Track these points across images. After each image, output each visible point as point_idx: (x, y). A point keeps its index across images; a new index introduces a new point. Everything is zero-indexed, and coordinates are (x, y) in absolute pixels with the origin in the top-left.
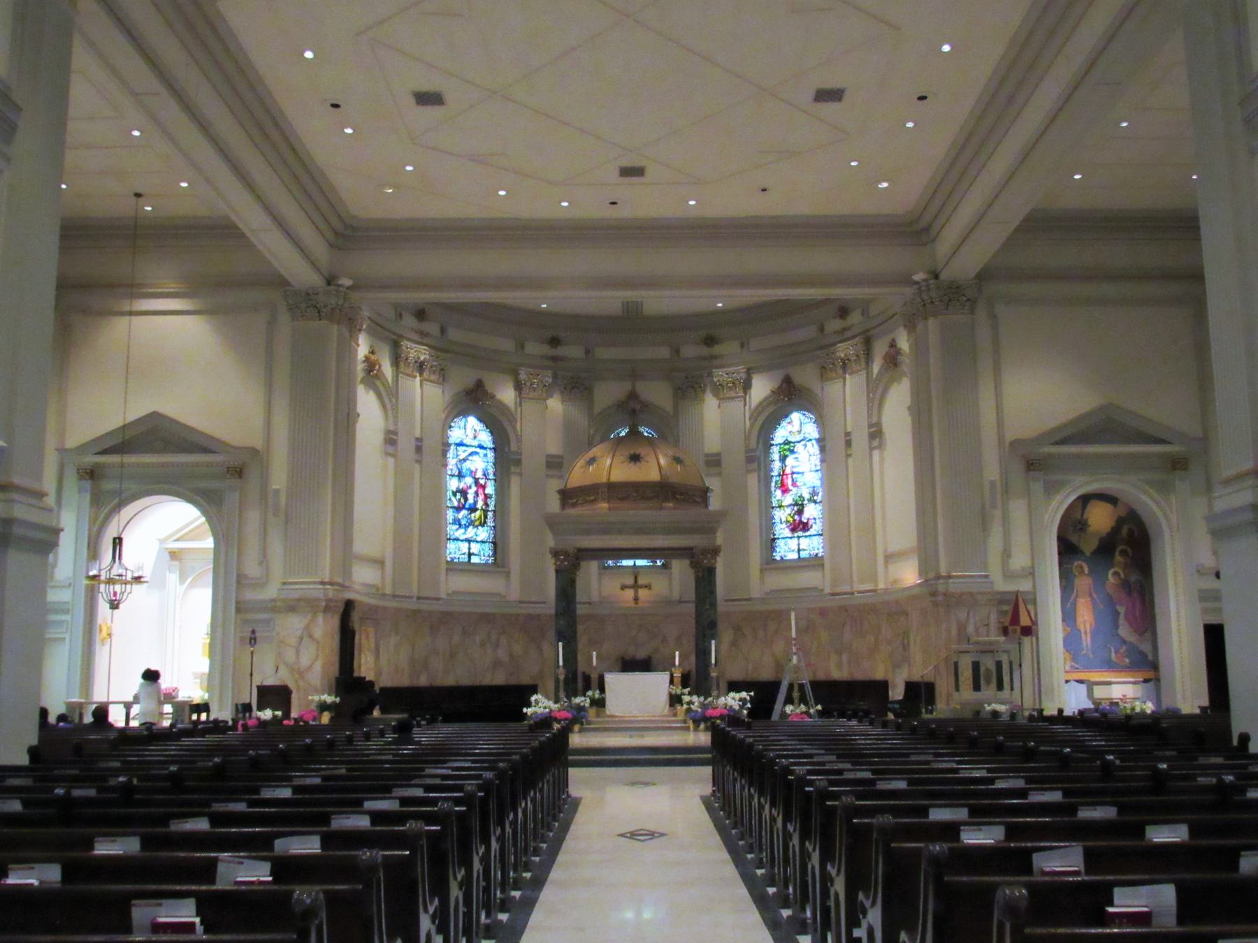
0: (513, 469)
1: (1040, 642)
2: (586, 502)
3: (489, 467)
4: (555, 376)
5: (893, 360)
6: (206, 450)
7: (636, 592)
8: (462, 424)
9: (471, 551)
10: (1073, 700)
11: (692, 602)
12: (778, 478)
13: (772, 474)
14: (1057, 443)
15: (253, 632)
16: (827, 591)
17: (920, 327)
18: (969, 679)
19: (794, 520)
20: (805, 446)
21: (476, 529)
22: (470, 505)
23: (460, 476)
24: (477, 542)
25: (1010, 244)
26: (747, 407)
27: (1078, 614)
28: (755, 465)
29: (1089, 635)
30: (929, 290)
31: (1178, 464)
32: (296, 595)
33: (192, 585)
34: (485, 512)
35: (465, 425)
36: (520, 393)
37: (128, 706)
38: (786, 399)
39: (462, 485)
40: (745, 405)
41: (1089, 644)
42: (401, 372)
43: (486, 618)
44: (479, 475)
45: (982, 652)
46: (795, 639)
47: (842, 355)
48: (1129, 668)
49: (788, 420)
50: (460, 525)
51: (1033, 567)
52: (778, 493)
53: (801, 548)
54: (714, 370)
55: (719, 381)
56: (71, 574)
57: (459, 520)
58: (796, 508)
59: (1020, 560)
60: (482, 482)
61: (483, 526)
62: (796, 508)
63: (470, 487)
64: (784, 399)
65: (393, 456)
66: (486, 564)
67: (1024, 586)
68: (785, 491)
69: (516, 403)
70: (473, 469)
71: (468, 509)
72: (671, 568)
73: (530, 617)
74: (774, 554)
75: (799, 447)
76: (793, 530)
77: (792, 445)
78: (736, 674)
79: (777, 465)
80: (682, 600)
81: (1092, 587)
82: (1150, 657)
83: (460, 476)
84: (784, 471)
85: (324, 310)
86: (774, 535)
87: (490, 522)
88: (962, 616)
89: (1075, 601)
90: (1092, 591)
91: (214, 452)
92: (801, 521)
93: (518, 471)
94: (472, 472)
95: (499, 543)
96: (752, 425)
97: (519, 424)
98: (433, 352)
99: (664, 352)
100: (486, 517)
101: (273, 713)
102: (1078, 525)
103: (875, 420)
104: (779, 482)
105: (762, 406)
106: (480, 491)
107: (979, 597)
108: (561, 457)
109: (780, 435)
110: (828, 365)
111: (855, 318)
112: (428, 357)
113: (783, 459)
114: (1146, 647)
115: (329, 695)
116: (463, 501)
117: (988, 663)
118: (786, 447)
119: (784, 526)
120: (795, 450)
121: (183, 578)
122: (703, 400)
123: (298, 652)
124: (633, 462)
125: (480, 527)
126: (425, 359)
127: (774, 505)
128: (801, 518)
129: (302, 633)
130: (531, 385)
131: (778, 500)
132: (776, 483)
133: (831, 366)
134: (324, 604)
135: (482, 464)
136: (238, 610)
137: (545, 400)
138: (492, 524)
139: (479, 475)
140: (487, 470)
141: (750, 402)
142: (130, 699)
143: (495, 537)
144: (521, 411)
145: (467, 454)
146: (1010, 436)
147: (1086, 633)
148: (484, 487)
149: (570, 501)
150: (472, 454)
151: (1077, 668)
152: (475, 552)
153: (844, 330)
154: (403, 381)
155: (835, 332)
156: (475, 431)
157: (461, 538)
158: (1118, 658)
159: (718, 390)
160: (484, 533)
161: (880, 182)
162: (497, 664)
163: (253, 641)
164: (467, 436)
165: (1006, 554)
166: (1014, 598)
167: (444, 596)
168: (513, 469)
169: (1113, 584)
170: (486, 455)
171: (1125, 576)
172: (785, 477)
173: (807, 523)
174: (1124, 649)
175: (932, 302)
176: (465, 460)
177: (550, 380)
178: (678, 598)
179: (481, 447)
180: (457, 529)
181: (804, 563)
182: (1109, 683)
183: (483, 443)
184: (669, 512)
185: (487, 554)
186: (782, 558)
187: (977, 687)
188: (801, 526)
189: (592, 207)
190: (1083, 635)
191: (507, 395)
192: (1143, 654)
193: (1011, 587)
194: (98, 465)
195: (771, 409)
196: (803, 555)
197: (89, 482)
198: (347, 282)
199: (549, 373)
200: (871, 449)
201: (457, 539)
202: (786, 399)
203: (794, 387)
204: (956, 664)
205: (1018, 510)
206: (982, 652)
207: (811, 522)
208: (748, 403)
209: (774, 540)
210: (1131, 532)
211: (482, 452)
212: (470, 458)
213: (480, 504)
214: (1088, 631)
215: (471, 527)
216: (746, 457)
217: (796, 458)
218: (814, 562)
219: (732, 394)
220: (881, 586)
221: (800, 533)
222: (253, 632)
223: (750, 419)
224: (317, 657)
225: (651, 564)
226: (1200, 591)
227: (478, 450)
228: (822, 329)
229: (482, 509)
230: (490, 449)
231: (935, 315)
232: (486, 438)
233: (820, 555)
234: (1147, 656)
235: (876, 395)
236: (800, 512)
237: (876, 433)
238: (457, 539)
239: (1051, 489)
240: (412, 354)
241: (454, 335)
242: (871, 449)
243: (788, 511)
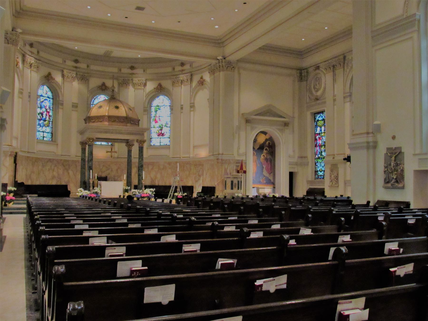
0: (60, 107)
1: (247, 176)
2: (99, 121)
3: (51, 105)
4: (77, 74)
5: (202, 82)
6: (281, 117)
7: (112, 154)
8: (42, 88)
9: (44, 136)
10: (252, 193)
11: (126, 158)
12: (154, 118)
13: (152, 116)
14: (255, 115)
16: (171, 156)
17: (216, 74)
18: (230, 186)
19: (159, 132)
20: (164, 107)
21: (46, 128)
22: (44, 119)
23: (41, 108)
24: (46, 132)
25: (256, 52)
26: (145, 93)
28: (146, 113)
29: (255, 174)
30: (222, 62)
31: (286, 124)
34: (49, 121)
35: (43, 89)
36: (64, 79)
38: (159, 91)
39: (41, 111)
40: (144, 91)
41: (255, 176)
42: (25, 67)
43: (50, 160)
44: (47, 108)
45: (234, 178)
46: (178, 172)
47: (182, 79)
48: (265, 184)
49: (158, 98)
50: (40, 126)
51: (246, 153)
52: (154, 122)
53: (161, 142)
54: (134, 78)
55: (135, 82)
57: (40, 124)
58: (160, 128)
59: (242, 150)
60: (48, 110)
61: (48, 127)
62: (160, 128)
63: (44, 112)
64: (158, 91)
65: (21, 98)
66: (49, 141)
67: (243, 158)
68: (156, 122)
69: (62, 83)
70: (46, 106)
71: (43, 120)
72: (115, 146)
73: (65, 161)
74: (151, 143)
75: (162, 108)
76: (159, 135)
77: (159, 107)
78: (148, 183)
79: (153, 114)
80: (119, 157)
82: (272, 181)
83: (41, 108)
84: (156, 115)
85: (10, 40)
86: (151, 137)
87: (50, 125)
88: (226, 167)
91: (284, 118)
92: (161, 133)
93: (62, 107)
94: (45, 106)
95: (53, 133)
96: (146, 99)
97: (63, 90)
98: (36, 60)
99: (115, 70)
100: (49, 124)
103: (192, 102)
104: (154, 119)
105: (150, 93)
106: (48, 114)
107: (231, 161)
108: (77, 104)
109: (156, 102)
110: (176, 82)
111: (187, 67)
112: (34, 62)
113: (156, 111)
114: (271, 178)
115: (12, 187)
116: (42, 117)
117: (235, 181)
118: (158, 107)
119: (155, 134)
120: (161, 109)
122: (129, 88)
124: (116, 109)
125: (47, 127)
126: (33, 62)
127: (152, 127)
128: (161, 132)
130: (68, 76)
131: (154, 125)
132: (153, 119)
133: (177, 82)
134: (10, 153)
135: (48, 104)
137: (72, 82)
138: (51, 126)
139: (47, 108)
140: (50, 106)
141: (146, 91)
143: (52, 131)
144: (64, 86)
145: (43, 99)
146: (242, 111)
148: (49, 112)
149: (92, 121)
150: (45, 100)
152: (46, 136)
153: (183, 70)
154: (26, 69)
155: (179, 71)
156: (46, 91)
157: (41, 131)
159: (134, 85)
160: (48, 129)
161: (216, 25)
162: (53, 177)
164: (44, 93)
165: (239, 148)
166: (241, 162)
167: (36, 152)
168: (60, 107)
170: (50, 101)
171: (266, 156)
172: (156, 117)
173: (164, 134)
174: (264, 178)
175: (223, 67)
176: (42, 102)
177: (75, 75)
178: (117, 157)
179: (48, 97)
180: (39, 127)
181: (161, 147)
182: (264, 188)
183: (49, 96)
184: (130, 128)
185: (49, 137)
186: (154, 145)
187: (232, 188)
188: (161, 134)
189: (119, 18)
191: (58, 78)
192: (270, 180)
193: (240, 158)
195: (154, 94)
196: (162, 144)
198: (19, 31)
199: (75, 73)
200: (190, 111)
201: (39, 131)
202: (159, 91)
203: (162, 87)
204: (226, 181)
205: (243, 134)
206: (234, 178)
207: (165, 134)
208: (145, 91)
209: (151, 138)
210: (269, 143)
211: (49, 99)
212: (44, 101)
213: (47, 119)
214: (255, 172)
215: (44, 127)
216: (144, 110)
217: (161, 111)
218: (167, 147)
219: (140, 87)
220: (191, 156)
221: (161, 137)
223: (145, 97)
225: (107, 144)
226: (289, 162)
227: (47, 98)
228: (174, 69)
229: (48, 121)
230: (51, 98)
231: (223, 71)
232: (50, 94)
233: (168, 144)
234: (271, 180)
235: (194, 94)
236: (161, 130)
237: (192, 106)
238: (39, 131)
239: (253, 129)
240: (29, 60)
241: (42, 54)
242: (190, 111)
243: (157, 129)
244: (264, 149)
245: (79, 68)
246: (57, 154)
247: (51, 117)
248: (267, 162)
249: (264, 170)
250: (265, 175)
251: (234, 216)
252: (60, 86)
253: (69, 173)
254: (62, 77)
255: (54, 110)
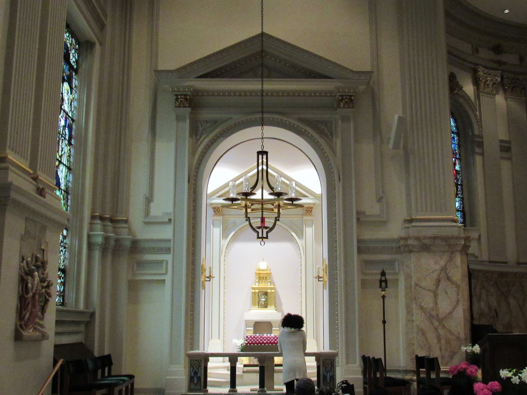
0: (477, 150)
11: (259, 217)
15: (383, 274)
32: (430, 233)
33: (234, 239)
36: (478, 89)
37: (233, 359)
56: (171, 210)
91: (326, 77)
95: (467, 209)
108: (509, 142)
121: (225, 234)
123: (436, 296)
129: (439, 275)
136: (360, 251)
137: (495, 95)
140: (455, 150)
142: (235, 350)
143: (463, 208)
163: (383, 284)
177: (499, 80)
194: (197, 93)
197: (189, 110)
222: (383, 274)
224: (458, 301)
245: (505, 63)
246: (479, 259)
247: (459, 174)
251: (212, 238)
252: (473, 103)
253: (508, 304)
254: (474, 85)
255: (463, 158)
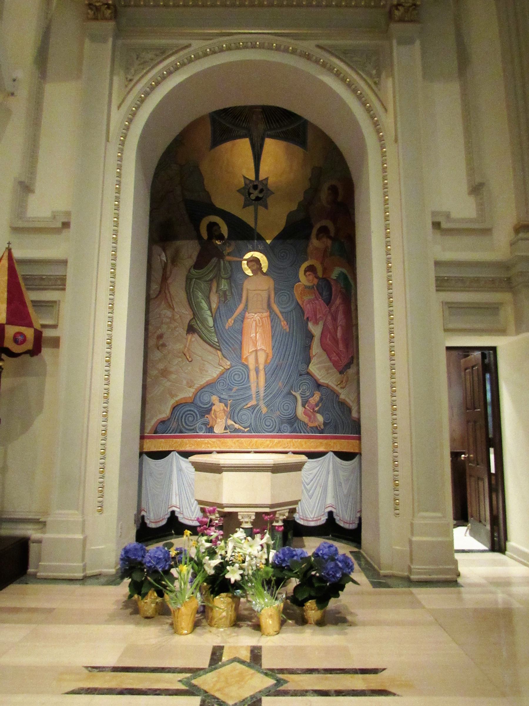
27: (246, 340)
81: (273, 295)
89: (242, 319)
90: (272, 300)
101: (240, 565)
102: (252, 191)
108: (68, 214)
147: (257, 371)
151: (236, 430)
158: (305, 413)
169: (306, 287)
174: (317, 397)
190: (253, 374)
214: (261, 367)
244: (314, 231)
248: (328, 302)
249: (316, 348)
250: (322, 381)
